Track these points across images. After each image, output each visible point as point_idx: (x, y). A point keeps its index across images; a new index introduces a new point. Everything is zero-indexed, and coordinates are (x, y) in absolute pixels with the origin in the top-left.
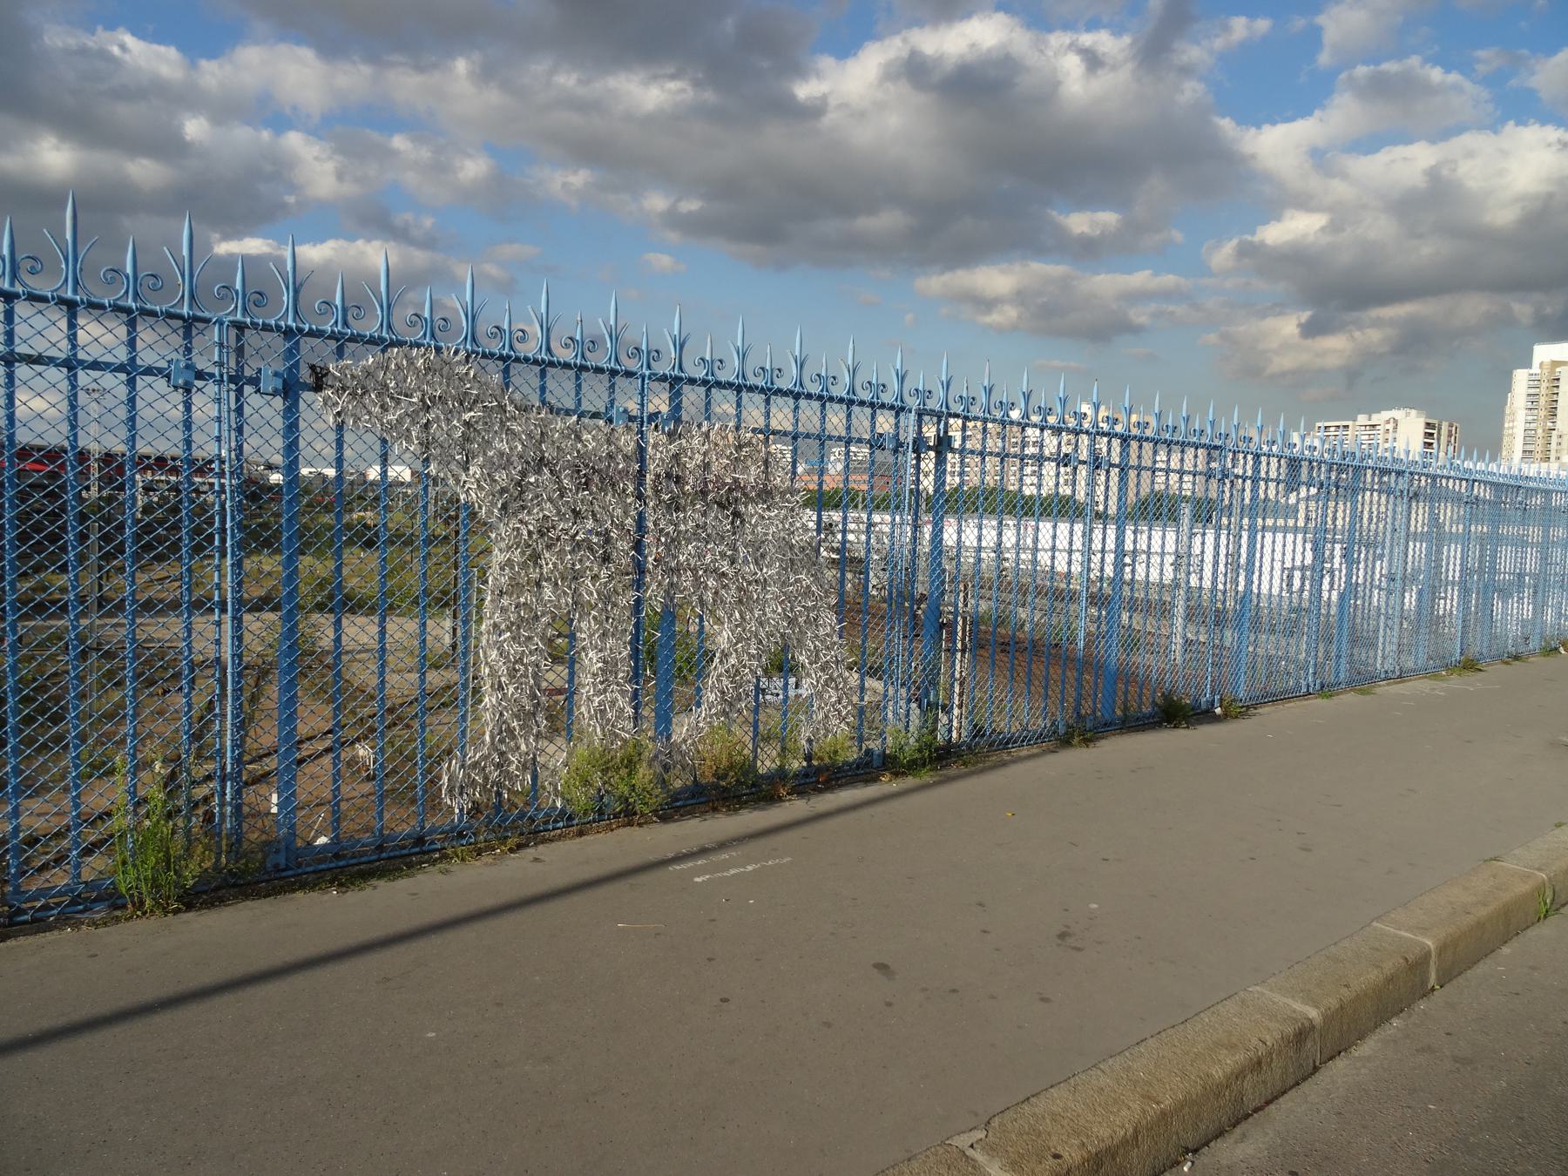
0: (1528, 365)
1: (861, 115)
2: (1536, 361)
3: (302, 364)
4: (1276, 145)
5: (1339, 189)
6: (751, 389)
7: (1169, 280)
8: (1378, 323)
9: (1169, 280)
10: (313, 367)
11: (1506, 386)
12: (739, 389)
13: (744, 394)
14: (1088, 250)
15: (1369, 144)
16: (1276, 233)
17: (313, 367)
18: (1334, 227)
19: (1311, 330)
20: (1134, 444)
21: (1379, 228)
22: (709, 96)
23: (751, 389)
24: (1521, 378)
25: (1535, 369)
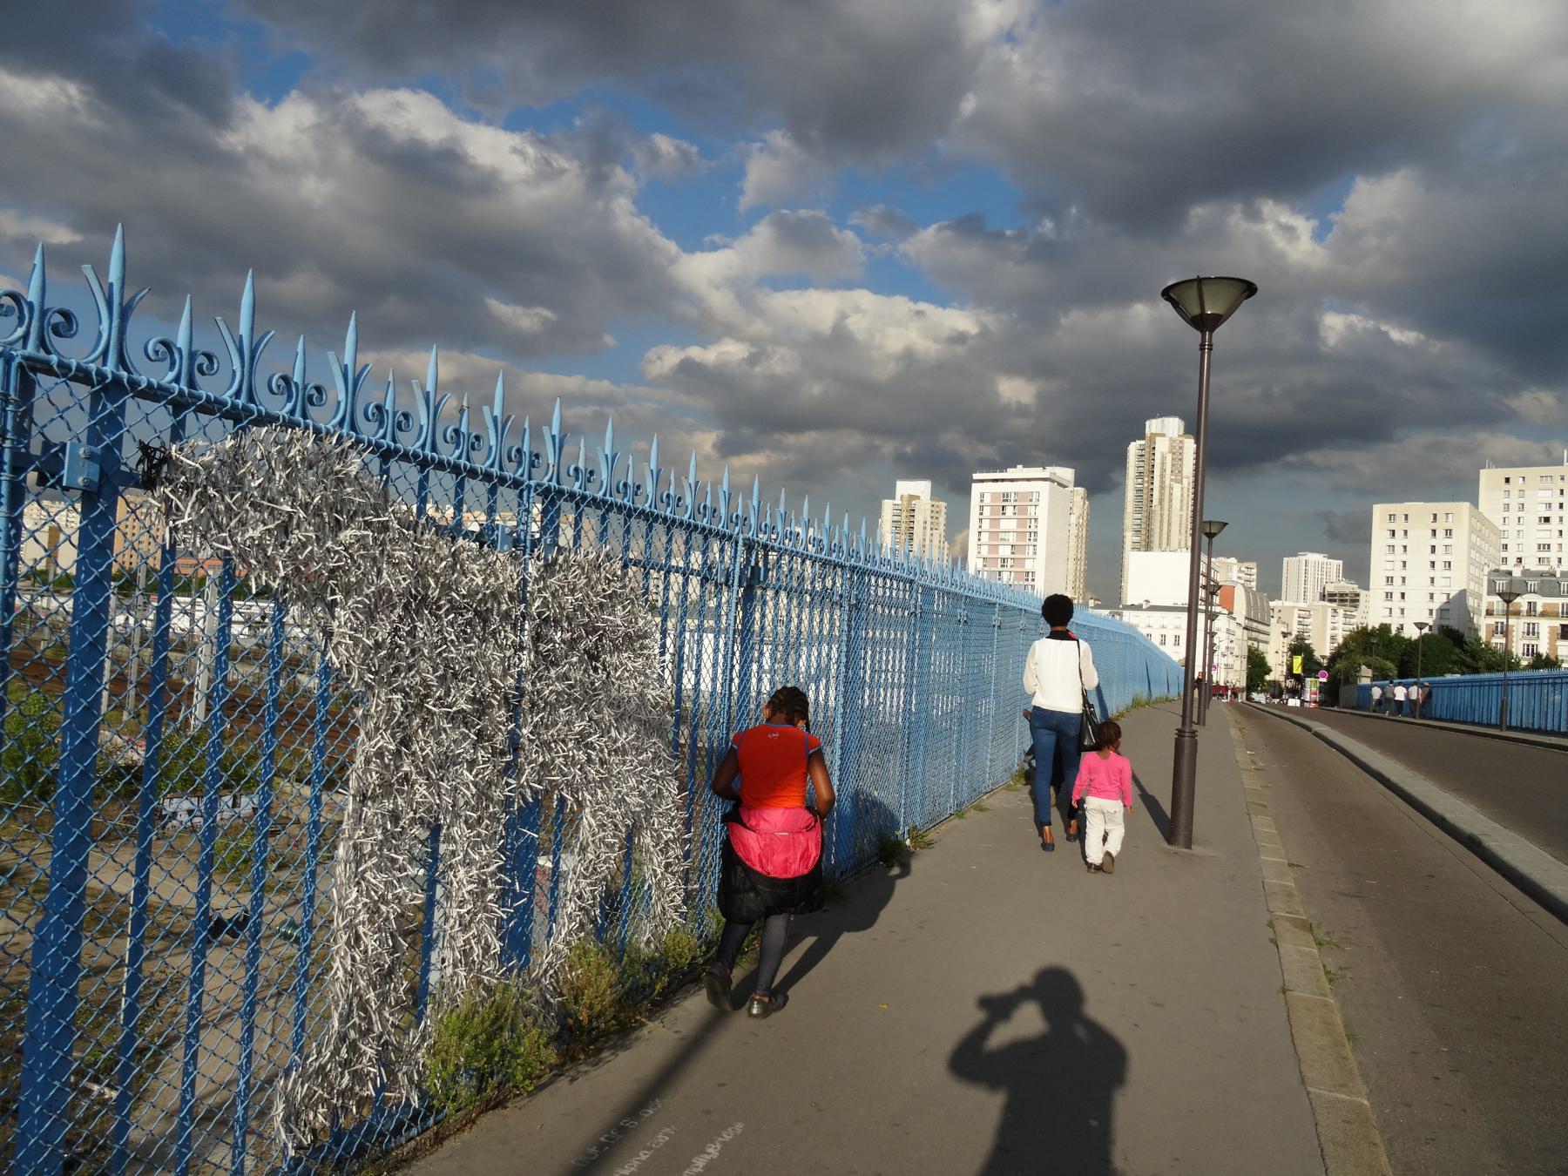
0: (893, 498)
1: (281, 167)
2: (898, 496)
3: (127, 439)
4: (704, 270)
5: (758, 327)
6: (441, 466)
7: (604, 386)
8: (777, 447)
9: (604, 386)
10: (144, 448)
11: (877, 513)
12: (424, 464)
13: (190, 416)
14: (522, 348)
15: (779, 283)
16: (708, 355)
17: (144, 448)
18: (753, 360)
19: (728, 448)
20: (566, 506)
21: (782, 363)
22: (96, 124)
23: (441, 466)
24: (887, 505)
25: (898, 501)
